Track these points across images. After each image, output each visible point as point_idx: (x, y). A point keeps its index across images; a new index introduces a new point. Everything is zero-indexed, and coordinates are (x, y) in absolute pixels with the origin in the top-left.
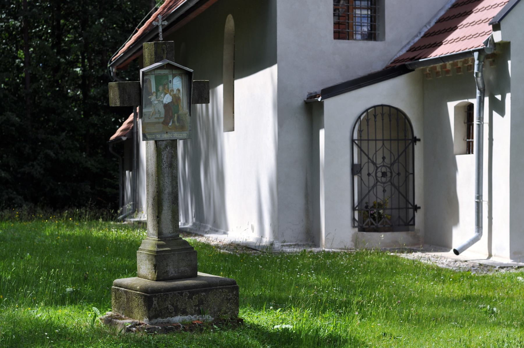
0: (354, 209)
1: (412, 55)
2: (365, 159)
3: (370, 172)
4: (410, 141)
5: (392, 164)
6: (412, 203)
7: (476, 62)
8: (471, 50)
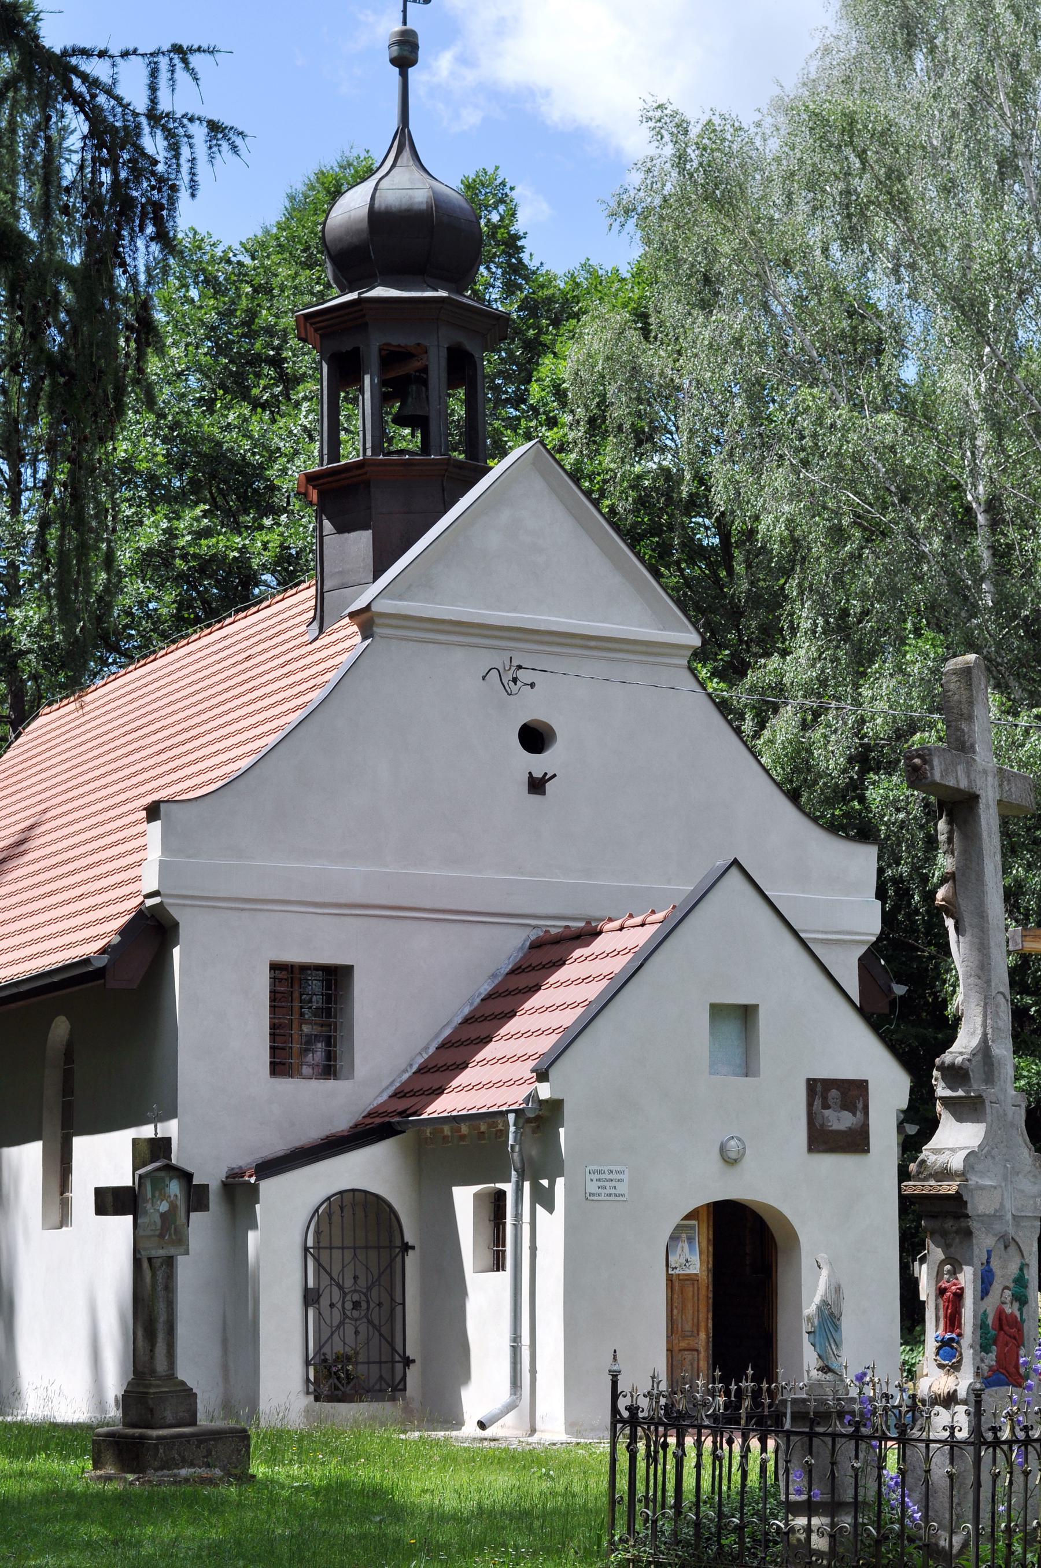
0: (307, 1363)
1: (402, 1105)
2: (325, 1280)
3: (334, 1301)
4: (397, 1250)
5: (369, 1288)
6: (401, 1353)
7: (512, 1129)
8: (504, 1108)
